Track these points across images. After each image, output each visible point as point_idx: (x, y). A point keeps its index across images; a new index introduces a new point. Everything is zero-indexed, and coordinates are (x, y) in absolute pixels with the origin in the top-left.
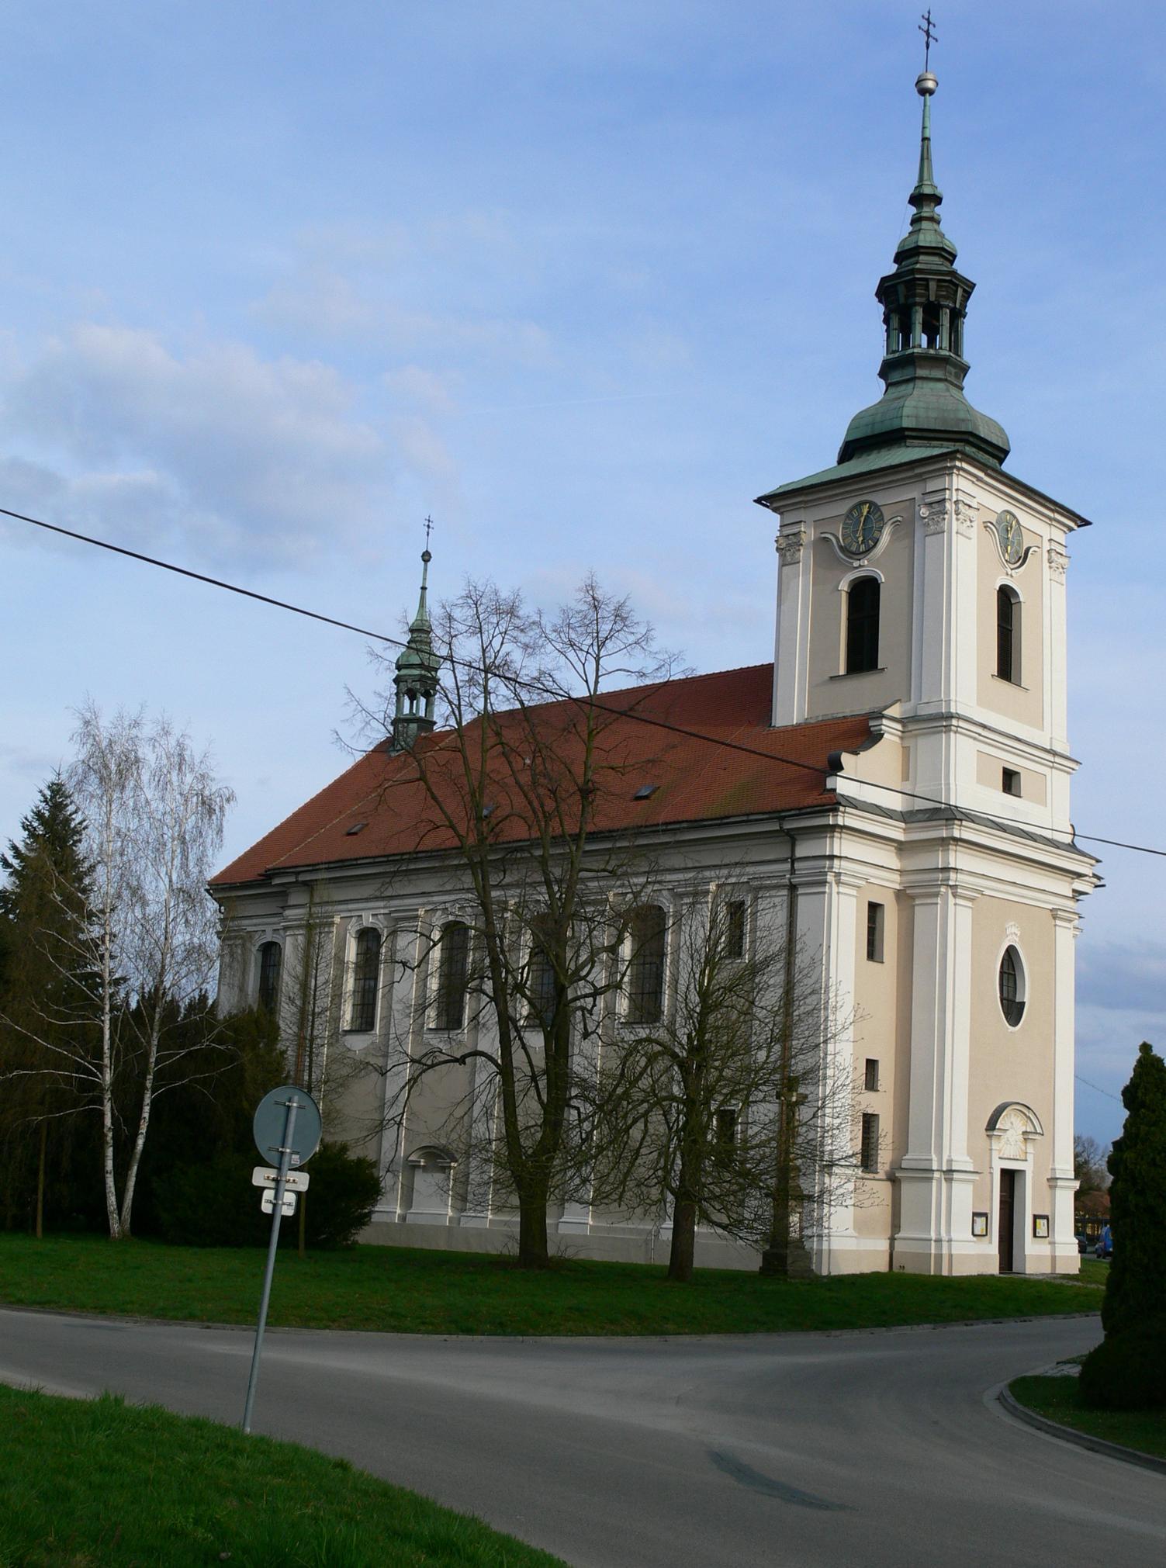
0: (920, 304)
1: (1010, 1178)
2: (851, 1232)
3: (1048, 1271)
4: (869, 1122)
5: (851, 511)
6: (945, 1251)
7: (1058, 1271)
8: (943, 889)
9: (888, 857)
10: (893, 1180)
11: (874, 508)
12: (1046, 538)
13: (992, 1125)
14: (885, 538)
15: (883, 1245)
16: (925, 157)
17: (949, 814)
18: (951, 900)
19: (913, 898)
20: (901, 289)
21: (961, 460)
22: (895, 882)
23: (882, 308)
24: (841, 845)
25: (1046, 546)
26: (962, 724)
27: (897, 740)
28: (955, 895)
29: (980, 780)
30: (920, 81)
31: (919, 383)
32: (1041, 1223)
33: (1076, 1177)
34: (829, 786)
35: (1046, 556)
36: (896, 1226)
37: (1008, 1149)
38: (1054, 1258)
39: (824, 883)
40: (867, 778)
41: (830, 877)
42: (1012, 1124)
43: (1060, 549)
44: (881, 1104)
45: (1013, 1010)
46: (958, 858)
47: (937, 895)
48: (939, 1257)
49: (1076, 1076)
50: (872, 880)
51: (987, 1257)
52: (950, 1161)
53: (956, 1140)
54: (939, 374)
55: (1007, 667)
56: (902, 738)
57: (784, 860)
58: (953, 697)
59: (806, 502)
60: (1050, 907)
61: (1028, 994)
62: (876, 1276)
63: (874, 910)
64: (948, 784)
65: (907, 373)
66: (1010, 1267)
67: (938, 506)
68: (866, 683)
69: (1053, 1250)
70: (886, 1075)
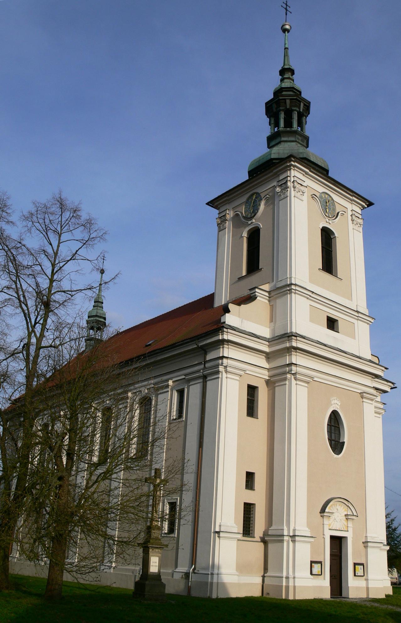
0: (283, 110)
1: (338, 543)
3: (364, 596)
4: (249, 508)
5: (248, 200)
6: (291, 584)
7: (297, 598)
8: (288, 376)
10: (264, 541)
11: (258, 194)
13: (323, 510)
14: (262, 207)
15: (260, 580)
16: (286, 55)
17: (289, 336)
19: (274, 383)
20: (274, 106)
21: (294, 162)
22: (265, 375)
23: (268, 119)
24: (227, 351)
26: (297, 288)
27: (267, 301)
28: (296, 379)
30: (283, 26)
31: (283, 143)
32: (360, 570)
34: (222, 321)
35: (350, 218)
36: (266, 569)
37: (336, 523)
38: (368, 589)
40: (247, 321)
41: (221, 369)
42: (338, 511)
43: (357, 215)
44: (258, 497)
45: (337, 445)
46: (296, 358)
47: (285, 379)
48: (287, 587)
49: (385, 487)
50: (247, 372)
51: (321, 588)
52: (294, 530)
53: (298, 515)
54: (293, 139)
55: (329, 264)
56: (269, 301)
57: (200, 364)
58: (293, 275)
59: (228, 200)
60: (359, 391)
61: (346, 438)
63: (252, 390)
65: (277, 141)
67: (284, 186)
69: (367, 584)
70: (260, 481)
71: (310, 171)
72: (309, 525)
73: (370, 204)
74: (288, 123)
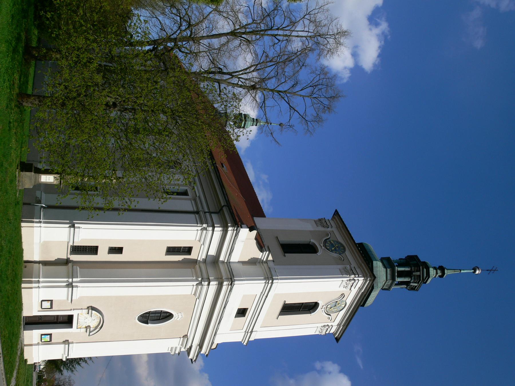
0: (411, 269)
2: (42, 241)
3: (26, 343)
5: (340, 243)
6: (34, 285)
9: (213, 252)
12: (333, 324)
13: (93, 309)
15: (36, 258)
17: (232, 281)
18: (195, 283)
25: (330, 324)
26: (270, 285)
28: (197, 284)
29: (245, 296)
31: (385, 269)
32: (47, 338)
33: (67, 359)
35: (326, 324)
37: (83, 319)
39: (202, 224)
40: (243, 245)
41: (205, 225)
42: (93, 320)
44: (103, 255)
46: (214, 285)
48: (31, 282)
52: (77, 287)
53: (88, 291)
54: (389, 277)
55: (289, 309)
60: (188, 335)
62: (21, 251)
63: (188, 250)
64: (244, 280)
66: (27, 324)
68: (279, 250)
71: (363, 293)
72: (81, 298)
73: (337, 340)
74: (401, 274)
